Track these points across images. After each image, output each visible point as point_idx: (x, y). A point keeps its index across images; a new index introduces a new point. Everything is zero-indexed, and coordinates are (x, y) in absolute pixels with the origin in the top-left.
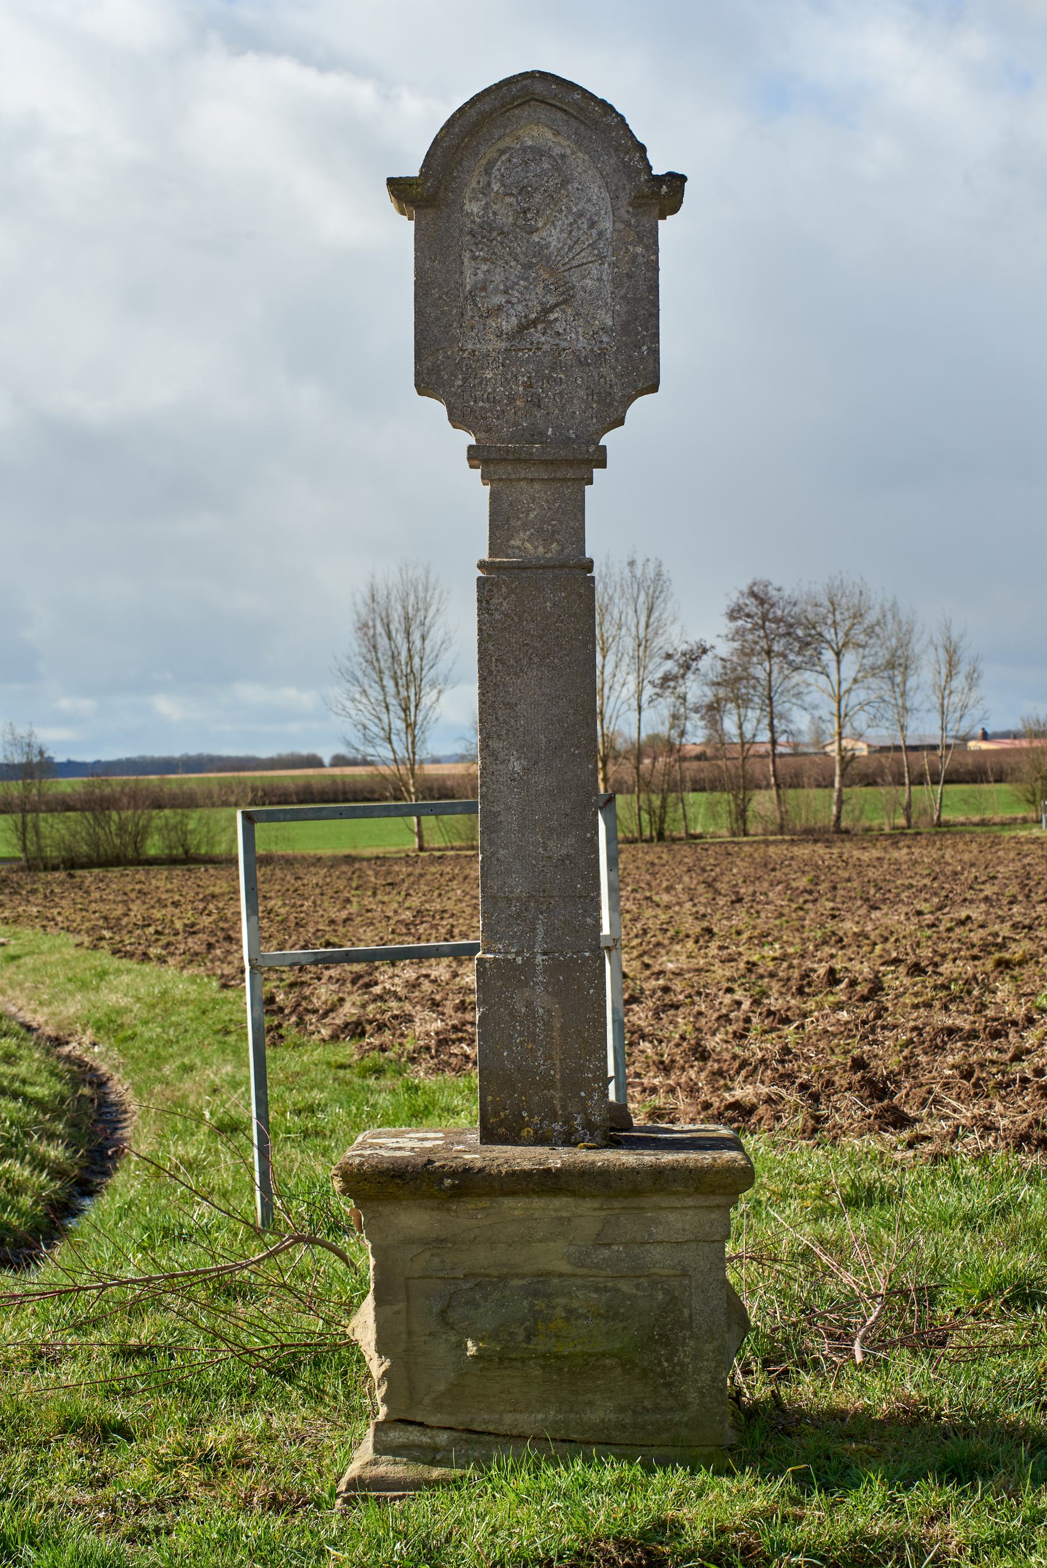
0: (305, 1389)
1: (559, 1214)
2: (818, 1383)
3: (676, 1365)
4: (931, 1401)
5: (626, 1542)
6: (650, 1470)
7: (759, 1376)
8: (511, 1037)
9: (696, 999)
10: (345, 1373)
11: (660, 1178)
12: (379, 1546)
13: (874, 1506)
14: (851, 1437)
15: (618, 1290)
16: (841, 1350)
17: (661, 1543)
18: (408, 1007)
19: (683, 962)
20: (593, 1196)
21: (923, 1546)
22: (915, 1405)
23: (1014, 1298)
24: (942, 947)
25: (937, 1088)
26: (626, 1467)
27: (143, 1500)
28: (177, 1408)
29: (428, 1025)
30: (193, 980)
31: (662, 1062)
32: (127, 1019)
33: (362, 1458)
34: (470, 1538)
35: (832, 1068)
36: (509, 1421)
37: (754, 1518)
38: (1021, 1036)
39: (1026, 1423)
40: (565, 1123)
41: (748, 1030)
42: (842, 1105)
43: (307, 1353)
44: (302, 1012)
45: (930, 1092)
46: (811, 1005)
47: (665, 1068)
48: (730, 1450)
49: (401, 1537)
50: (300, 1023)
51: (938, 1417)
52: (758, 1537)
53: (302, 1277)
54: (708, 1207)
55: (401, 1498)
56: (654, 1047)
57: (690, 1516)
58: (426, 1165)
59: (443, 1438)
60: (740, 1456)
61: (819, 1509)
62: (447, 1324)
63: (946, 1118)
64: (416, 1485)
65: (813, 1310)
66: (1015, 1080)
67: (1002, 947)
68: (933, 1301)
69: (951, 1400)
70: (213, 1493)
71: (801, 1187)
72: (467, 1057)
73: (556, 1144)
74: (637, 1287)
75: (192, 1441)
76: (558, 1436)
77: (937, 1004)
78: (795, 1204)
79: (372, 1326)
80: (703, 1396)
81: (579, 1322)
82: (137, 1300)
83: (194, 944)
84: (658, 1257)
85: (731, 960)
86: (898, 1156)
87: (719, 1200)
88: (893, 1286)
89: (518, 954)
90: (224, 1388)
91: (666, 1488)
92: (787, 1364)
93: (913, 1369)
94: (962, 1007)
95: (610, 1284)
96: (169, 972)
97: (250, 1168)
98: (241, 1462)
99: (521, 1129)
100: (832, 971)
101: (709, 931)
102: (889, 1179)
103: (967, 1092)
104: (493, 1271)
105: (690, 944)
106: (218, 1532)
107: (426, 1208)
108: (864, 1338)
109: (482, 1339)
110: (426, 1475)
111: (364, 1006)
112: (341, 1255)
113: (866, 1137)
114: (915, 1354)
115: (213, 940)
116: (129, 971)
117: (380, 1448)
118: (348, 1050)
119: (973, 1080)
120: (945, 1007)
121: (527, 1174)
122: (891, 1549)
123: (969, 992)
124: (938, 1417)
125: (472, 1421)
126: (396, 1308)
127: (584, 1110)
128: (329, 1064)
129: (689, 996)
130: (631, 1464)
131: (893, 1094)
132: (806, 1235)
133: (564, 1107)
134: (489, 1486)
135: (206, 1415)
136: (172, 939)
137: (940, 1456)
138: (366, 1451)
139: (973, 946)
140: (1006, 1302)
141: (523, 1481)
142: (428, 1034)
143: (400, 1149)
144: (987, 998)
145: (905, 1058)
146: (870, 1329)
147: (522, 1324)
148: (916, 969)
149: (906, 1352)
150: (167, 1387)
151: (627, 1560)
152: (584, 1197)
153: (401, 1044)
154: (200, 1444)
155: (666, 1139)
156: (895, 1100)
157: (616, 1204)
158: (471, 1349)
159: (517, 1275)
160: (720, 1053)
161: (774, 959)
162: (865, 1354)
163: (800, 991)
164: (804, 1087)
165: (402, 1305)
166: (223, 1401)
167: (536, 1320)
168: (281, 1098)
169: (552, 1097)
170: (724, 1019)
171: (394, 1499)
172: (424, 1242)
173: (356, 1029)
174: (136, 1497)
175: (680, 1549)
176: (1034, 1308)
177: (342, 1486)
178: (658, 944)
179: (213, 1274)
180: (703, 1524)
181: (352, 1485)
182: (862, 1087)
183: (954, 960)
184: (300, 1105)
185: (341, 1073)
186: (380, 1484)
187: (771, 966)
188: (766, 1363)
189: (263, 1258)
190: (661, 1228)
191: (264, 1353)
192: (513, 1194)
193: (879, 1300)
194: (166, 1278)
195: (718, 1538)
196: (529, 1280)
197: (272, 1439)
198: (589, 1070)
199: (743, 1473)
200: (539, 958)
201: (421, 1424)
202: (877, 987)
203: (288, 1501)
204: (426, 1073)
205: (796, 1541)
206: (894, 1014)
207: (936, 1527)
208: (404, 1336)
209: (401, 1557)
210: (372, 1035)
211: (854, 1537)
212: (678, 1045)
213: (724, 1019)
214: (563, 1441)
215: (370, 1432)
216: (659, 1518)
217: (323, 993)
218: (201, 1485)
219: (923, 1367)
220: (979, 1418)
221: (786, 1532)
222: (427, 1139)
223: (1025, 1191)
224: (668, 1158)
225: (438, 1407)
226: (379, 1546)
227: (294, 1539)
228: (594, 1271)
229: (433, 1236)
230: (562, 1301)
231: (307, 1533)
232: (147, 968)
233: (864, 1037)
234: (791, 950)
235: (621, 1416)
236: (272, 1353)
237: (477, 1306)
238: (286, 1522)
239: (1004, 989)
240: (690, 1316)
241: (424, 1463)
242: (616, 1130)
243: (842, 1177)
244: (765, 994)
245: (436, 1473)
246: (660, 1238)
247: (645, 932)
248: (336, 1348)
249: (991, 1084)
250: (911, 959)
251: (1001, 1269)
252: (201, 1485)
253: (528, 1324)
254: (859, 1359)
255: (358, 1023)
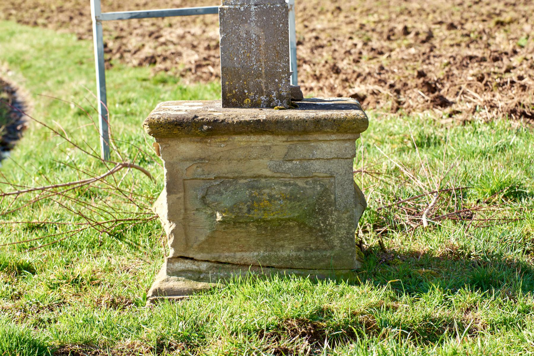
0: (129, 243)
1: (265, 144)
2: (404, 237)
3: (327, 225)
4: (464, 248)
5: (303, 320)
6: (315, 282)
7: (372, 234)
8: (238, 50)
9: (333, 43)
10: (151, 234)
11: (318, 125)
12: (170, 324)
13: (436, 302)
14: (422, 266)
15: (296, 185)
16: (415, 220)
17: (321, 321)
18: (179, 48)
19: (325, 24)
20: (283, 135)
21: (463, 323)
22: (456, 250)
23: (509, 194)
24: (466, 15)
25: (464, 87)
26: (302, 280)
27: (41, 305)
28: (60, 255)
29: (190, 57)
30: (62, 35)
31: (315, 75)
32: (26, 57)
33: (161, 279)
34: (219, 319)
35: (406, 77)
36: (239, 256)
37: (371, 307)
38: (510, 61)
39: (518, 260)
40: (267, 96)
41: (360, 58)
42: (412, 96)
43: (130, 224)
44: (122, 52)
45: (460, 88)
46: (394, 45)
47: (318, 78)
48: (357, 271)
49: (182, 319)
50: (122, 57)
51: (469, 256)
52: (373, 318)
53: (127, 186)
54: (343, 140)
55: (181, 299)
56: (311, 67)
57: (336, 306)
58: (194, 118)
59: (204, 266)
60: (363, 275)
61: (406, 303)
62: (205, 204)
63: (470, 102)
64: (190, 292)
65: (399, 200)
66: (507, 83)
67: (499, 15)
68: (464, 196)
69: (476, 247)
70: (80, 300)
71: (391, 138)
72: (211, 74)
73: (263, 107)
74: (306, 183)
75: (68, 272)
76: (265, 265)
77: (463, 45)
78: (388, 146)
79: (166, 206)
80: (342, 242)
81: (276, 202)
82: (37, 200)
83: (63, 17)
84: (317, 167)
85: (351, 22)
86: (443, 122)
87: (349, 136)
88: (443, 187)
89: (241, 5)
90: (85, 244)
91: (323, 292)
92: (387, 228)
93: (455, 231)
94: (477, 46)
95: (292, 182)
96: (49, 31)
97: (97, 132)
98: (94, 282)
99: (244, 99)
100: (405, 28)
101: (339, 9)
102: (439, 133)
103: (481, 88)
104: (230, 175)
105: (329, 15)
106: (83, 320)
107: (194, 142)
108: (428, 214)
109: (224, 212)
110: (195, 287)
111: (155, 48)
112: (147, 174)
113: (425, 112)
114: (455, 223)
115: (72, 15)
116: (27, 32)
117: (171, 273)
118: (148, 71)
119: (484, 82)
120: (468, 46)
121: (248, 123)
122: (446, 325)
123: (481, 38)
124: (469, 256)
125: (219, 257)
126: (178, 196)
127: (277, 89)
128: (137, 79)
129: (329, 41)
130: (304, 278)
131: (440, 90)
132: (395, 161)
133: (267, 88)
134: (229, 292)
135: (75, 259)
136: (50, 14)
137: (471, 276)
138: (163, 274)
139: (482, 15)
140: (505, 196)
141: (247, 288)
142: (190, 62)
143: (180, 110)
144: (491, 41)
145: (447, 72)
146: (431, 210)
147: (246, 204)
148: (452, 26)
149: (451, 222)
150: (54, 244)
151: (303, 330)
152: (278, 135)
153: (176, 68)
154: (72, 273)
155: (321, 105)
156: (442, 93)
157: (295, 139)
158: (219, 217)
159: (242, 177)
160: (346, 70)
161: (375, 22)
162: (428, 222)
163: (389, 38)
164: (392, 86)
165: (181, 195)
166: (85, 251)
167: (253, 201)
168: (112, 96)
169: (260, 82)
170: (348, 52)
171: (178, 300)
172: (192, 160)
173: (152, 60)
174: (37, 303)
175: (332, 324)
176: (520, 200)
177: (150, 293)
178: (312, 16)
179: (78, 185)
180: (344, 311)
181: (155, 293)
182: (423, 86)
183: (473, 22)
184: (123, 99)
185: (144, 83)
186: (170, 292)
187: (373, 26)
188: (375, 227)
189: (105, 176)
190: (319, 151)
191: (107, 225)
192: (240, 133)
193: (435, 194)
194: (53, 187)
195: (352, 318)
196: (249, 180)
197: (111, 270)
198: (280, 67)
199: (364, 284)
200: (253, 8)
201: (192, 259)
202: (430, 36)
203: (121, 302)
204: (190, 82)
205: (394, 320)
206: (439, 50)
207: (470, 314)
208: (183, 211)
209: (182, 330)
210: (160, 63)
211: (426, 318)
212: (324, 66)
213: (348, 52)
214: (268, 267)
215: (165, 264)
216: (320, 307)
217: (133, 42)
218: (73, 295)
219: (460, 230)
220: (492, 257)
221: (389, 315)
222: (194, 106)
223: (514, 139)
224: (322, 114)
225: (201, 249)
226: (170, 324)
227: (124, 321)
228: (284, 175)
229: (198, 156)
230: (267, 191)
231: (131, 319)
232: (37, 30)
233: (424, 61)
234: (383, 18)
235: (299, 253)
236: (111, 224)
237: (222, 194)
238: (120, 313)
239: (500, 36)
240: (335, 199)
241: (194, 280)
242: (295, 100)
243: (414, 134)
244: (369, 40)
245: (201, 285)
246: (318, 157)
247: (305, 9)
248: (145, 221)
249: (494, 84)
250: (449, 21)
251: (501, 178)
252: (73, 295)
253: (249, 203)
254: (425, 225)
255: (153, 57)
